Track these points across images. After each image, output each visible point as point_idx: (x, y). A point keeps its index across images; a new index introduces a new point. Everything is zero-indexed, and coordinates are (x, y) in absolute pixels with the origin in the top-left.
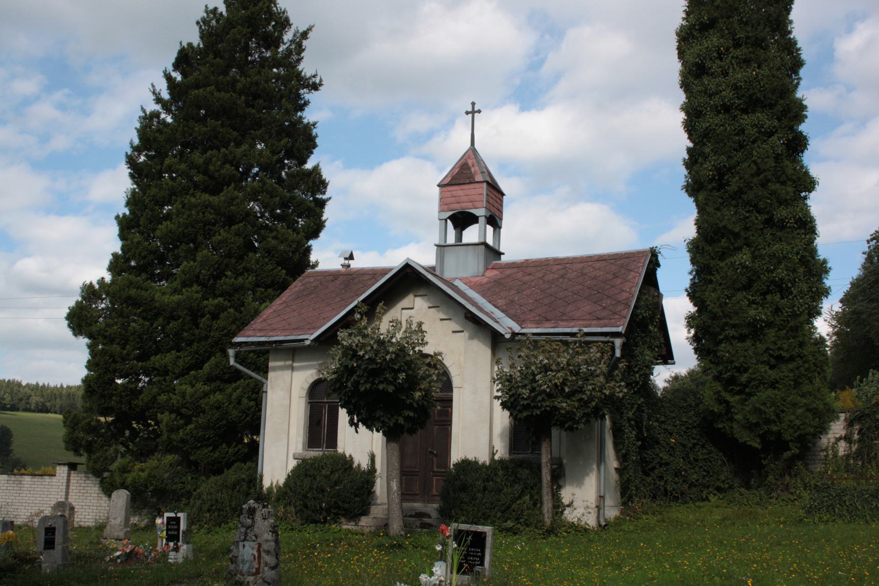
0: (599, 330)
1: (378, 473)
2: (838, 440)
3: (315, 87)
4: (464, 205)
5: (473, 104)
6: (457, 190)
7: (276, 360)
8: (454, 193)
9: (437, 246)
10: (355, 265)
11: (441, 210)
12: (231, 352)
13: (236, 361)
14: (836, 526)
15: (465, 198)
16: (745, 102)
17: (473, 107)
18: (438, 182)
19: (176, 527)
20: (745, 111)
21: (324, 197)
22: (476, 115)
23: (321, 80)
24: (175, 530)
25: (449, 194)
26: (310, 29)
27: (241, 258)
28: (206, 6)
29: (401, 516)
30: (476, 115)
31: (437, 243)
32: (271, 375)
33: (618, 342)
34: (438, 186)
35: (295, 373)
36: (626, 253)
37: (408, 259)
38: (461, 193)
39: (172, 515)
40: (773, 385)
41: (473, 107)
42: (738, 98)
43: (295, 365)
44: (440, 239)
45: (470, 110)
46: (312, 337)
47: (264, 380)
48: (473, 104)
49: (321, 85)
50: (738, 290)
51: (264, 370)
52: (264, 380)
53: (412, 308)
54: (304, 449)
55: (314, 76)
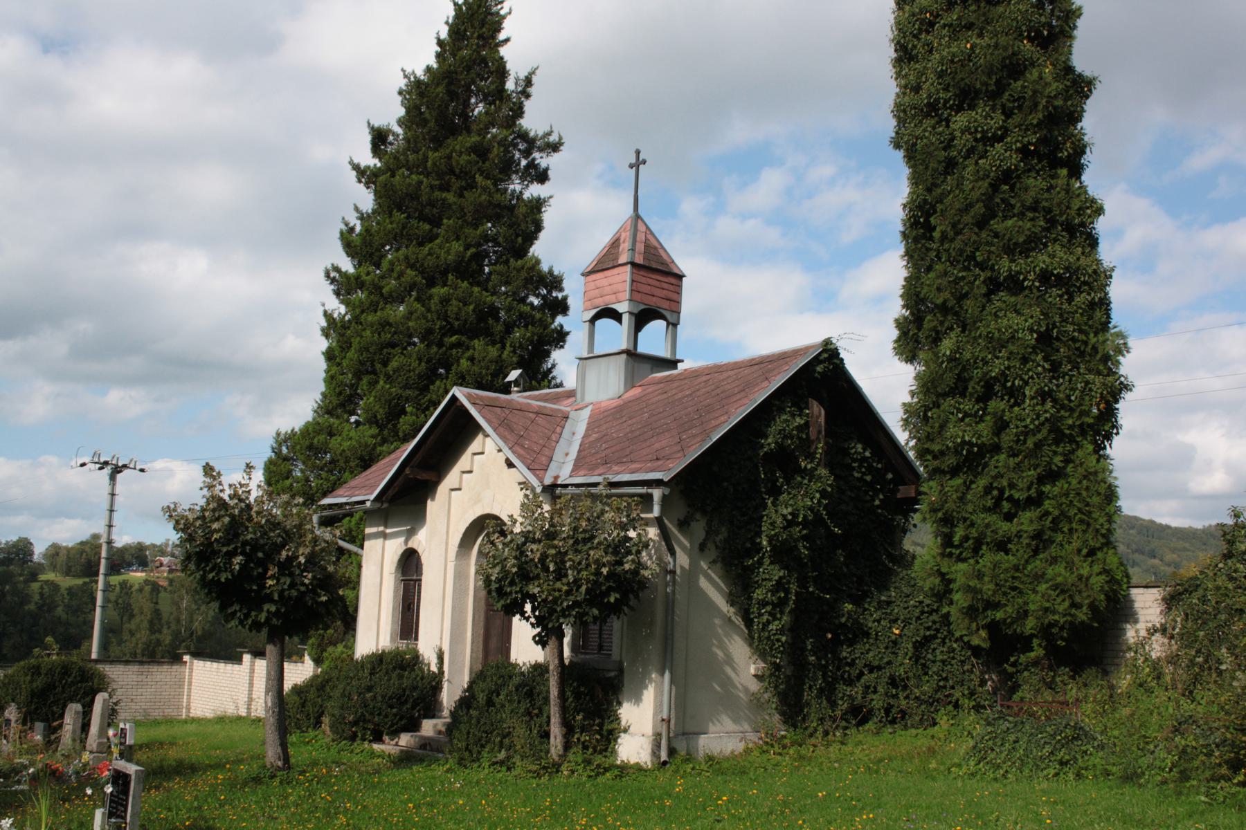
1: (446, 675)
2: (1152, 631)
3: (555, 147)
5: (638, 152)
7: (371, 526)
8: (598, 283)
14: (867, 776)
15: (608, 290)
16: (955, 95)
20: (959, 109)
23: (560, 138)
26: (533, 73)
27: (425, 389)
28: (403, 70)
32: (367, 544)
33: (657, 493)
34: (583, 275)
35: (387, 542)
36: (768, 356)
38: (605, 282)
40: (1002, 546)
42: (946, 89)
43: (388, 531)
46: (372, 497)
47: (360, 551)
48: (638, 152)
49: (561, 144)
50: (945, 395)
51: (358, 539)
52: (360, 551)
53: (482, 453)
54: (393, 640)
55: (549, 134)
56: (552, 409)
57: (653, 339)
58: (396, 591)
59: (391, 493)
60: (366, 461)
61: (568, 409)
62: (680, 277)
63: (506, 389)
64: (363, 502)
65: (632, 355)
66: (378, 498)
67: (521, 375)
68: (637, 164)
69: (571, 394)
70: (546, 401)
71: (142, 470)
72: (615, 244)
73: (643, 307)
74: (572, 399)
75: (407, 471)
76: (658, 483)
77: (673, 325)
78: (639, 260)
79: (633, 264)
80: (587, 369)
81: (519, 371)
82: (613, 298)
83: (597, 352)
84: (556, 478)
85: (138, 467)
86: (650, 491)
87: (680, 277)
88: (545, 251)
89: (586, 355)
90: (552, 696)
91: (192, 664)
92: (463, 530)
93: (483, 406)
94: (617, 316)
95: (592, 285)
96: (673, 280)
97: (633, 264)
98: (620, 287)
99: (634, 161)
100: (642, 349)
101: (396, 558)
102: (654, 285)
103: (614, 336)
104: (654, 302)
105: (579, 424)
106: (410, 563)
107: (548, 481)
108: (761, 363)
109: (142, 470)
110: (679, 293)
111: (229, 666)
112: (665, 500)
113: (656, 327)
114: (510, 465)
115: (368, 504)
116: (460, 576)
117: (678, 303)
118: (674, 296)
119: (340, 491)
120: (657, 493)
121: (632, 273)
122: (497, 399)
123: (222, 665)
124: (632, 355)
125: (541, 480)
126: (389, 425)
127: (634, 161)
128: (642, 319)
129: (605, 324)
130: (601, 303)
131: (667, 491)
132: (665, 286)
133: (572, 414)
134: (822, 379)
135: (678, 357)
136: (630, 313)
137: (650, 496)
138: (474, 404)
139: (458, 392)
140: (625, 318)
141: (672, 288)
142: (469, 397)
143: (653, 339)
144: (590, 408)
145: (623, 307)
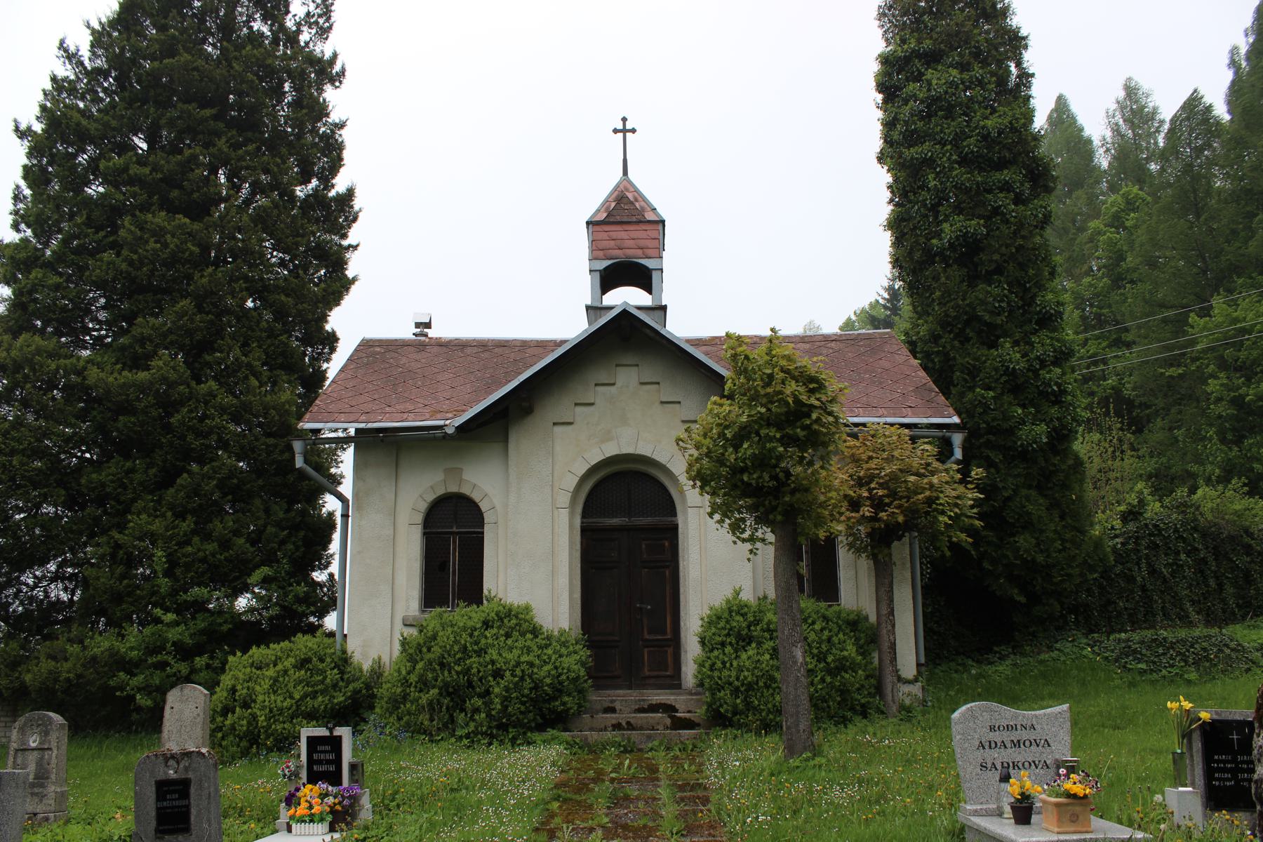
0: (925, 421)
4: (630, 252)
5: (624, 120)
6: (619, 233)
8: (614, 235)
9: (588, 308)
10: (432, 333)
11: (593, 258)
12: (298, 446)
13: (306, 461)
15: (630, 243)
17: (624, 125)
18: (587, 218)
19: (332, 757)
21: (345, 243)
22: (628, 135)
24: (329, 762)
25: (605, 236)
29: (245, 761)
30: (628, 135)
31: (589, 303)
33: (957, 439)
37: (625, 303)
38: (623, 235)
39: (322, 732)
41: (624, 125)
44: (593, 298)
45: (620, 127)
46: (459, 421)
48: (624, 120)
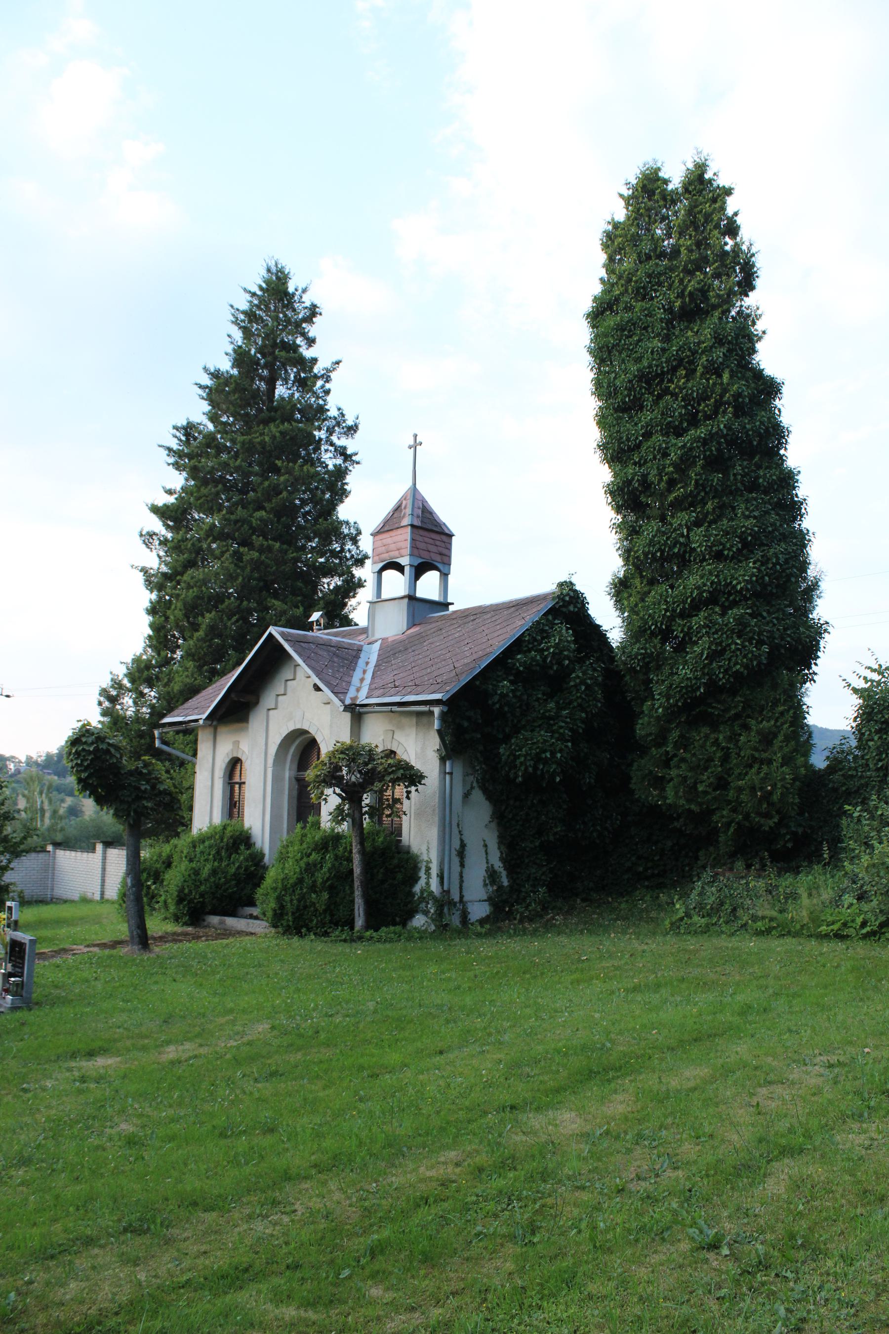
5: (416, 436)
8: (385, 541)
33: (437, 710)
34: (372, 535)
46: (204, 716)
48: (416, 436)
56: (350, 644)
57: (429, 586)
58: (224, 792)
59: (220, 713)
60: (191, 692)
61: (362, 643)
62: (450, 536)
63: (309, 627)
64: (197, 721)
65: (411, 598)
66: (208, 718)
67: (321, 616)
68: (415, 445)
69: (364, 631)
70: (344, 637)
71: (8, 696)
72: (398, 508)
73: (420, 561)
74: (364, 636)
75: (233, 695)
76: (437, 702)
77: (445, 575)
78: (417, 523)
79: (412, 526)
80: (376, 604)
81: (320, 613)
82: (396, 553)
83: (384, 596)
84: (356, 698)
85: (5, 694)
86: (432, 709)
87: (450, 536)
88: (344, 511)
89: (376, 600)
90: (355, 875)
91: (55, 853)
92: (279, 741)
93: (295, 642)
94: (400, 568)
95: (379, 543)
96: (444, 538)
97: (412, 526)
98: (403, 544)
99: (412, 443)
100: (419, 594)
101: (224, 766)
102: (428, 541)
103: (395, 584)
104: (427, 557)
105: (372, 654)
106: (235, 763)
107: (348, 702)
108: (517, 605)
109: (8, 696)
110: (450, 549)
111: (85, 855)
112: (443, 715)
113: (431, 579)
114: (317, 688)
115: (201, 722)
116: (277, 779)
117: (449, 557)
118: (445, 551)
119: (176, 712)
120: (437, 710)
121: (412, 533)
122: (305, 636)
123: (79, 854)
124: (411, 598)
125: (342, 701)
126: (209, 665)
127: (412, 443)
128: (419, 570)
129: (390, 575)
130: (387, 558)
131: (446, 709)
132: (438, 543)
133: (366, 647)
134: (568, 605)
135: (449, 601)
136: (411, 566)
137: (431, 713)
138: (287, 640)
139: (272, 630)
140: (407, 570)
141: (443, 545)
142: (283, 635)
143: (429, 586)
144: (379, 642)
145: (404, 561)
